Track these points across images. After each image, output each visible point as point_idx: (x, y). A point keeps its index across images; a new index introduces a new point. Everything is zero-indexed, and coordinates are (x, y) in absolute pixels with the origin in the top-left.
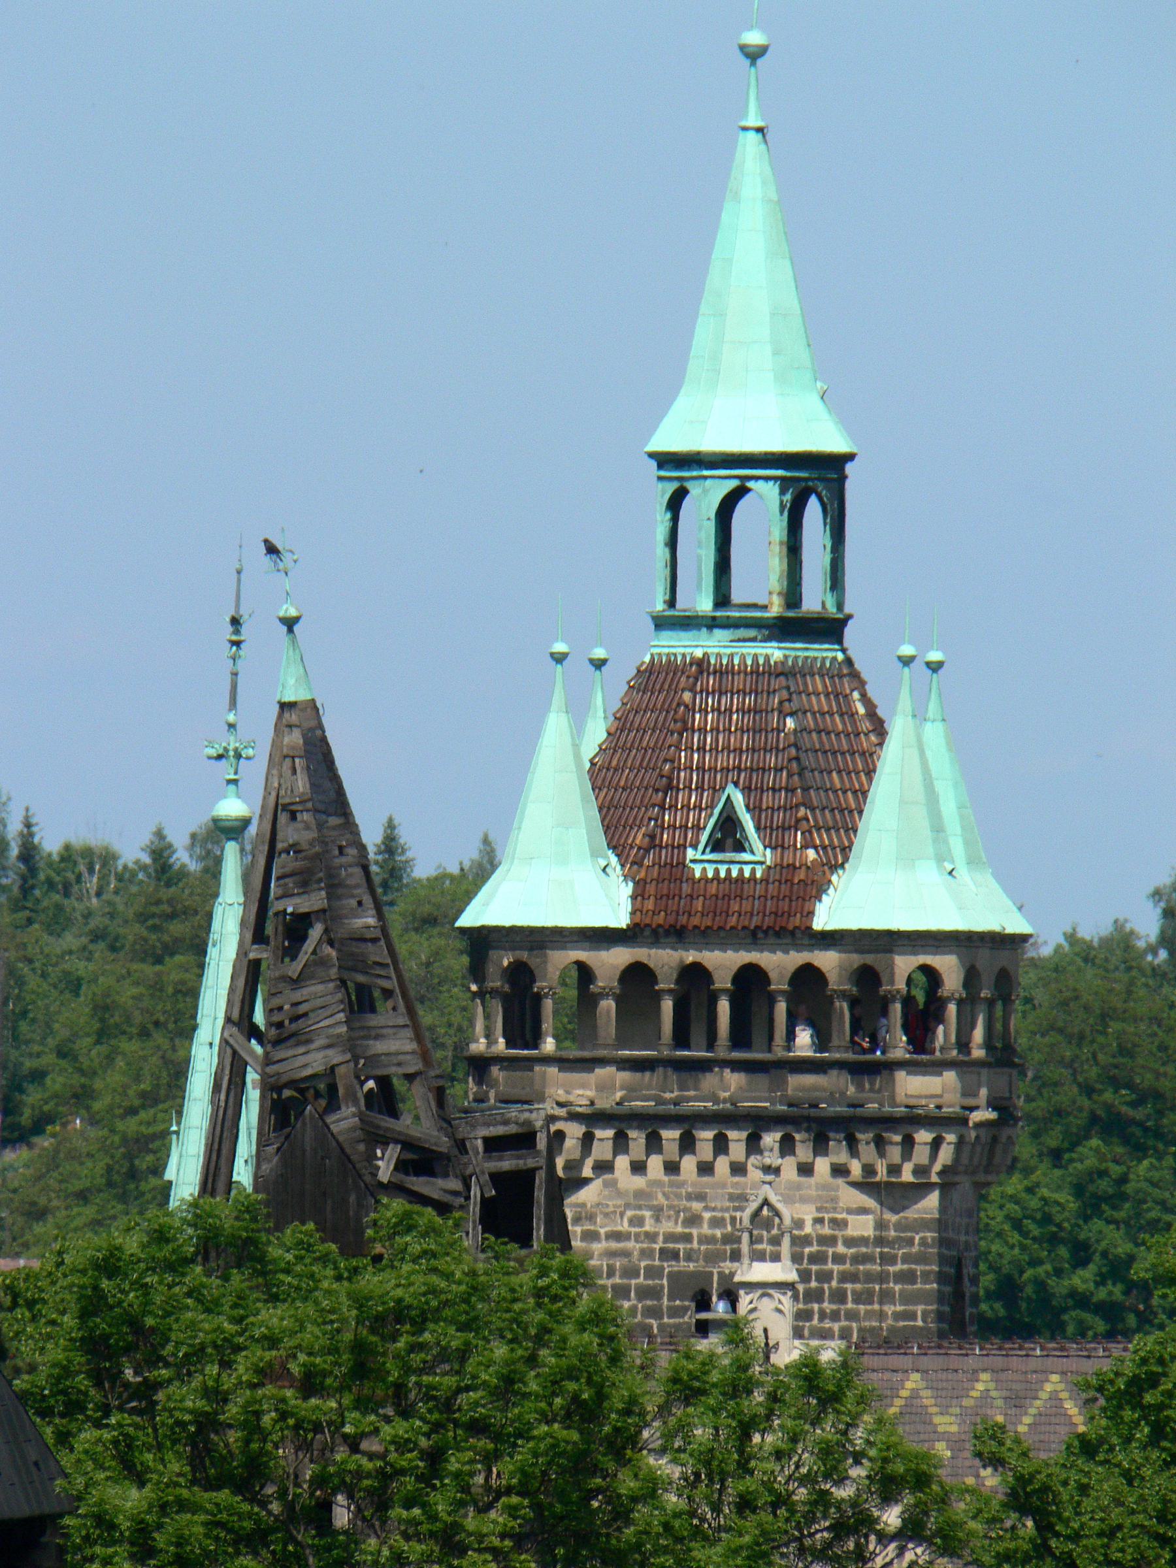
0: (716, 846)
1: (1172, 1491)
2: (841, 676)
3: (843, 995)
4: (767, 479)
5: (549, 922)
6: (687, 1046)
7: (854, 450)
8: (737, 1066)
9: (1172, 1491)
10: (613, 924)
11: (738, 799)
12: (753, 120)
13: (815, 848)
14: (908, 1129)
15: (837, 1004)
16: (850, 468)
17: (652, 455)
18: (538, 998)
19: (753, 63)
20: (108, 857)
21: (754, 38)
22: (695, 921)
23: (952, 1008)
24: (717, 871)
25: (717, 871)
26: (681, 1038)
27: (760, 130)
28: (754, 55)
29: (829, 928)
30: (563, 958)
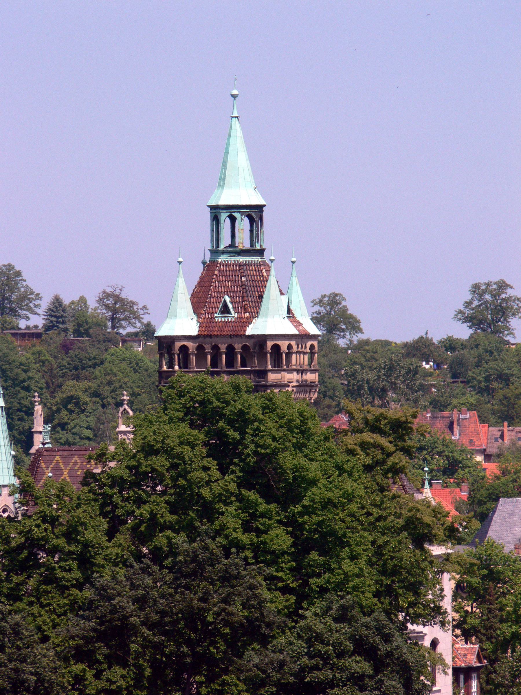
0: (222, 312)
1: (3, 603)
2: (260, 265)
3: (193, 353)
4: (237, 212)
5: (175, 335)
6: (246, 367)
7: (265, 203)
8: (229, 373)
9: (3, 603)
10: (193, 335)
11: (228, 299)
12: (236, 114)
13: (249, 312)
14: (281, 388)
15: (191, 356)
16: (264, 208)
17: (208, 206)
18: (281, 354)
19: (235, 99)
20: (471, 334)
21: (235, 92)
22: (215, 333)
23: (284, 355)
24: (222, 319)
25: (222, 319)
26: (243, 365)
27: (237, 117)
28: (234, 96)
29: (250, 334)
30: (178, 345)
